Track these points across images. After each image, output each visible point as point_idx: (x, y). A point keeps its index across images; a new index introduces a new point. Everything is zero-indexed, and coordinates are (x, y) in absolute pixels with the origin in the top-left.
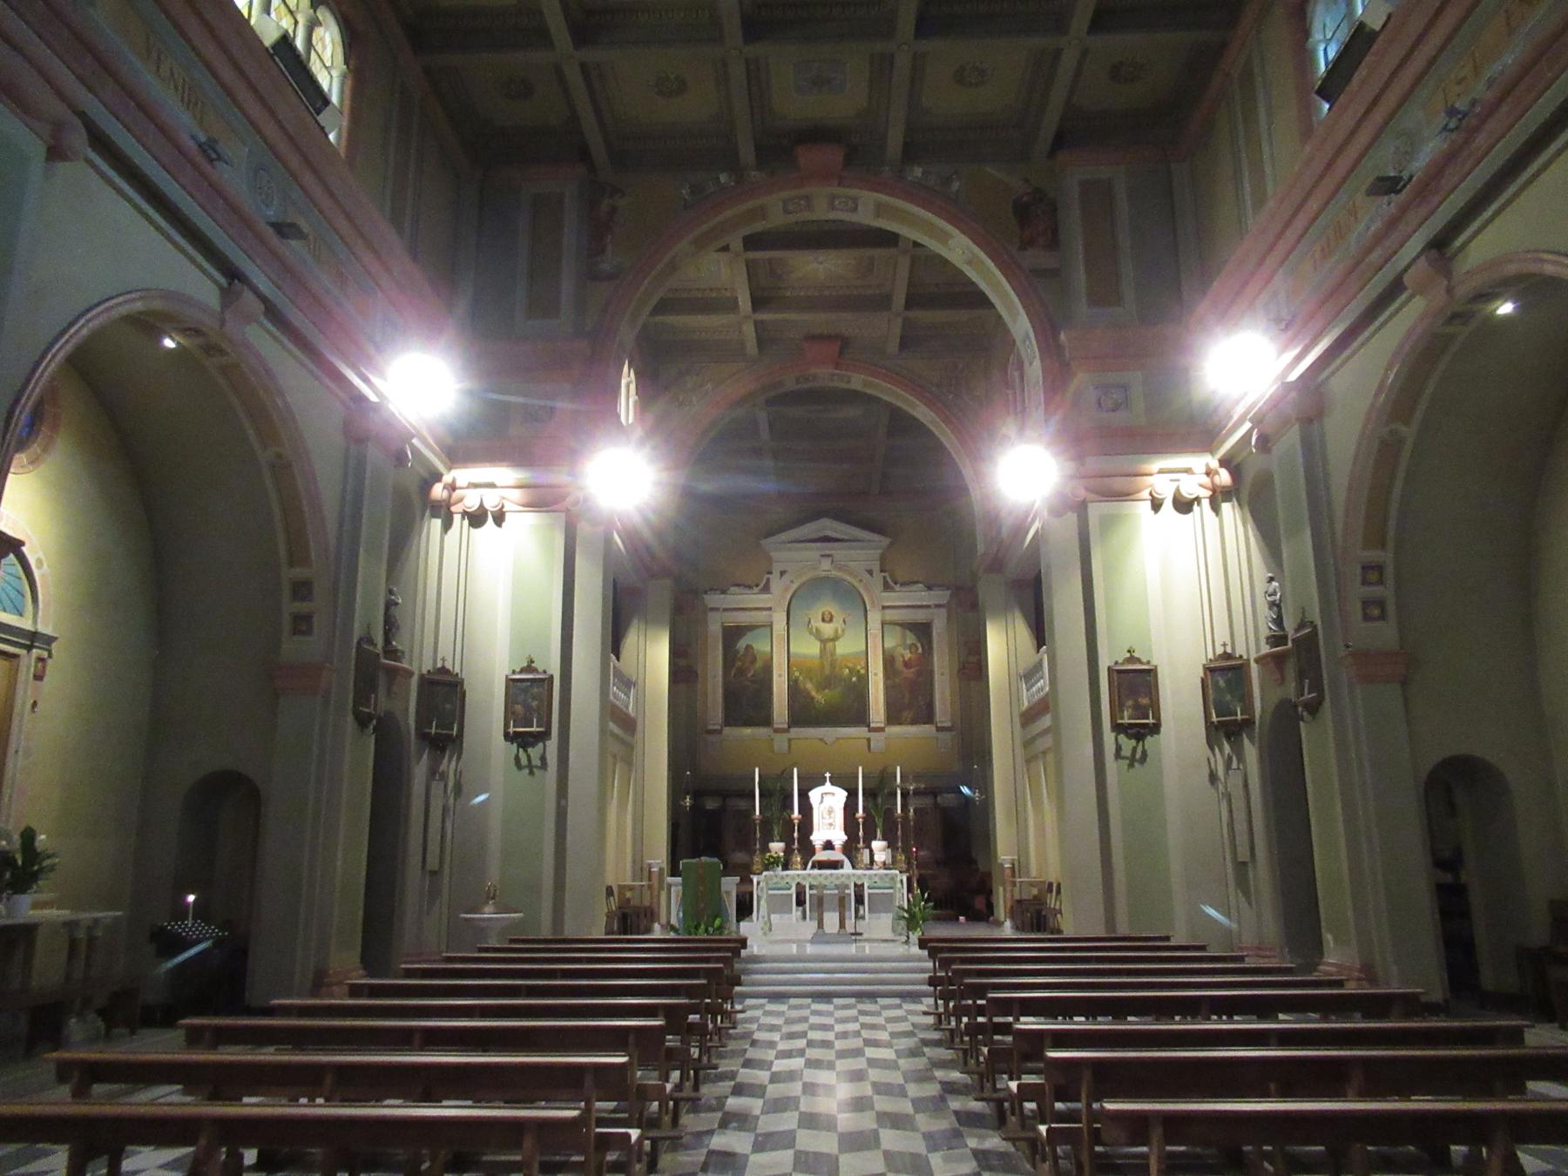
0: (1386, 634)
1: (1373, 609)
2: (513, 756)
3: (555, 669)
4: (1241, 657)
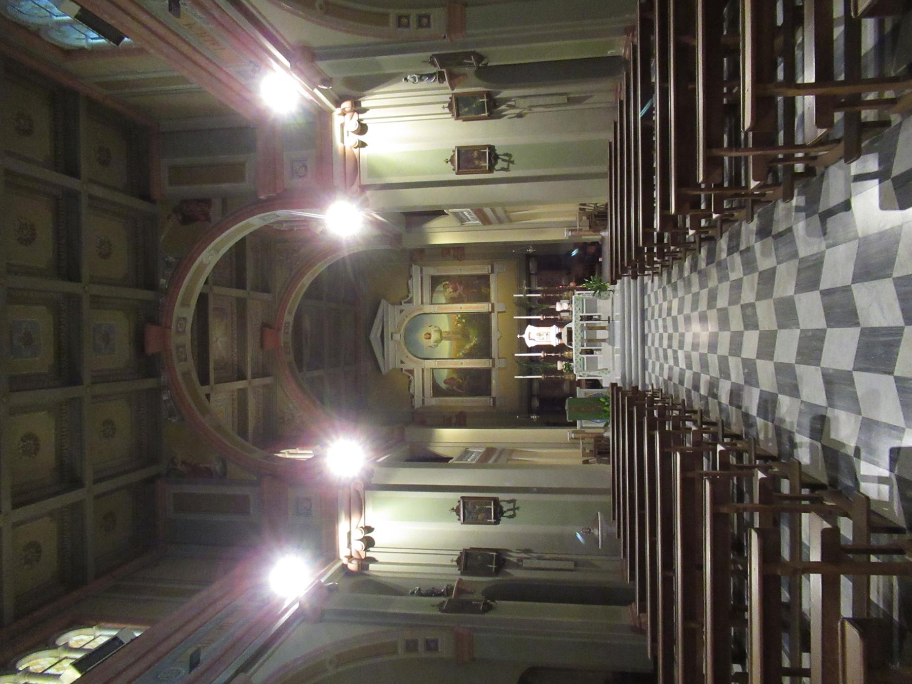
1: (423, 21)
3: (457, 496)
4: (450, 98)
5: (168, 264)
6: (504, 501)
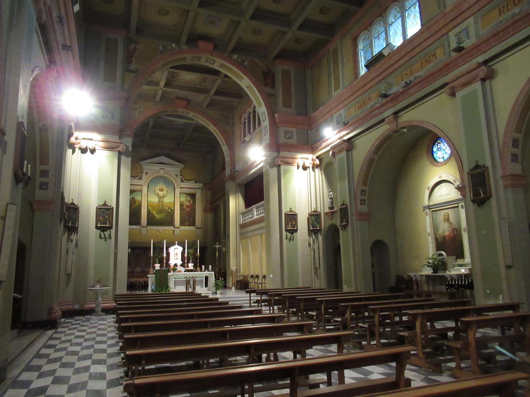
0: (364, 209)
1: (363, 202)
2: (99, 234)
3: (114, 205)
4: (319, 212)
5: (244, 61)
6: (110, 233)
